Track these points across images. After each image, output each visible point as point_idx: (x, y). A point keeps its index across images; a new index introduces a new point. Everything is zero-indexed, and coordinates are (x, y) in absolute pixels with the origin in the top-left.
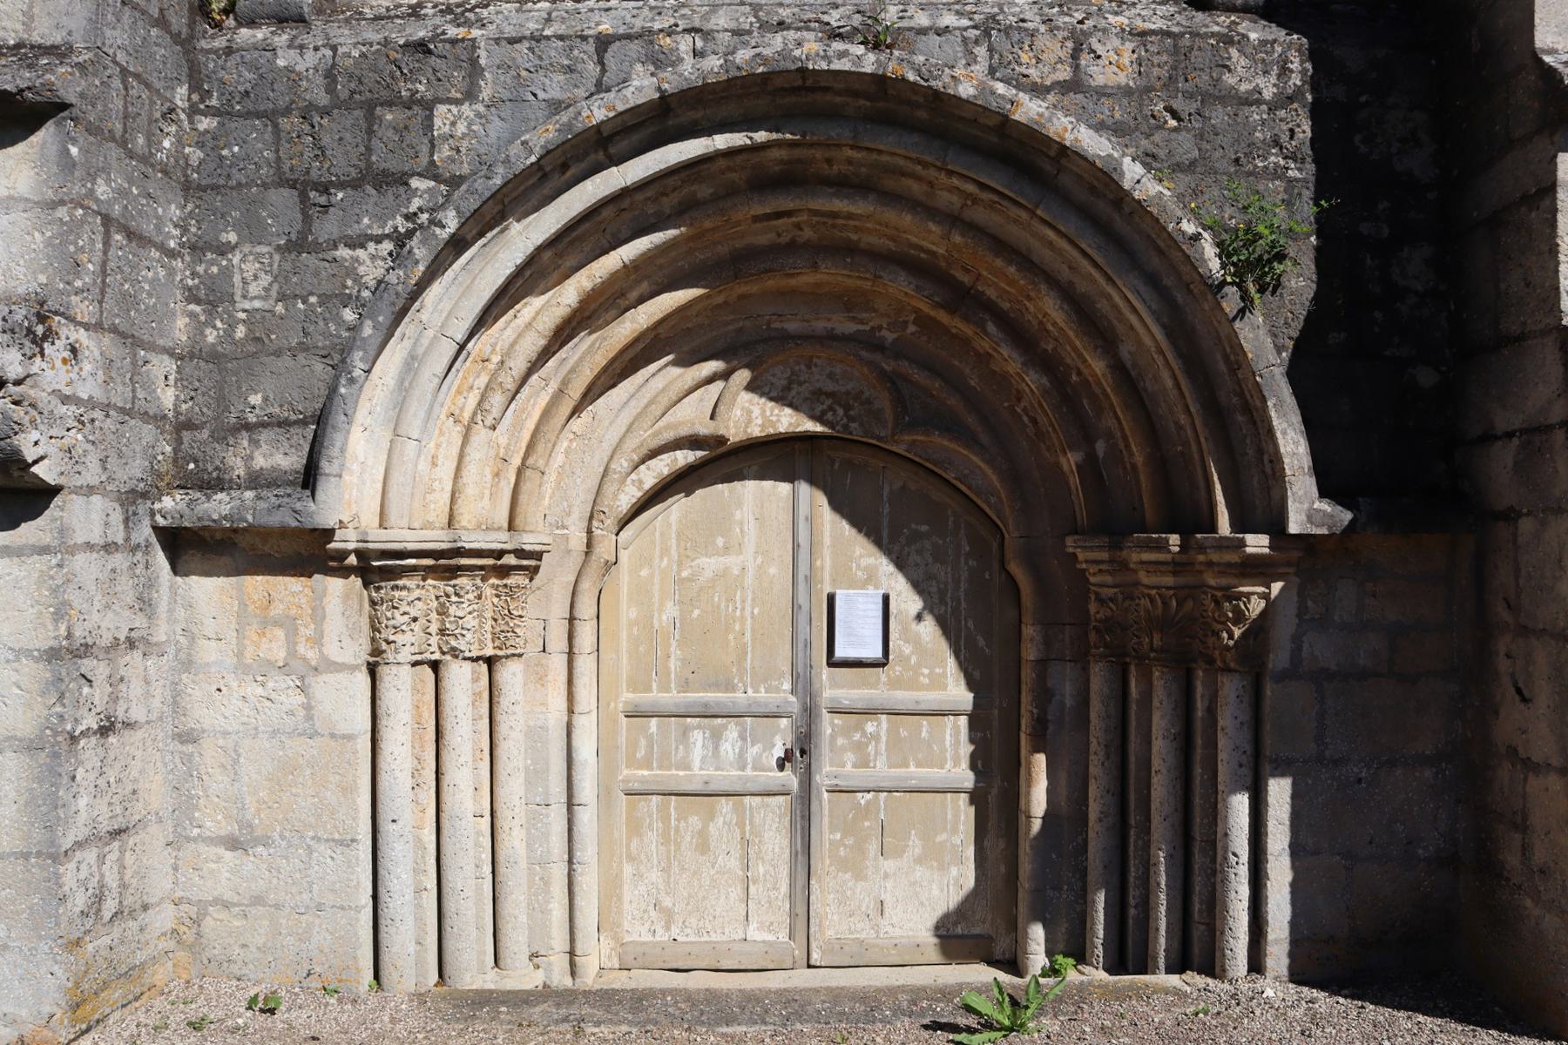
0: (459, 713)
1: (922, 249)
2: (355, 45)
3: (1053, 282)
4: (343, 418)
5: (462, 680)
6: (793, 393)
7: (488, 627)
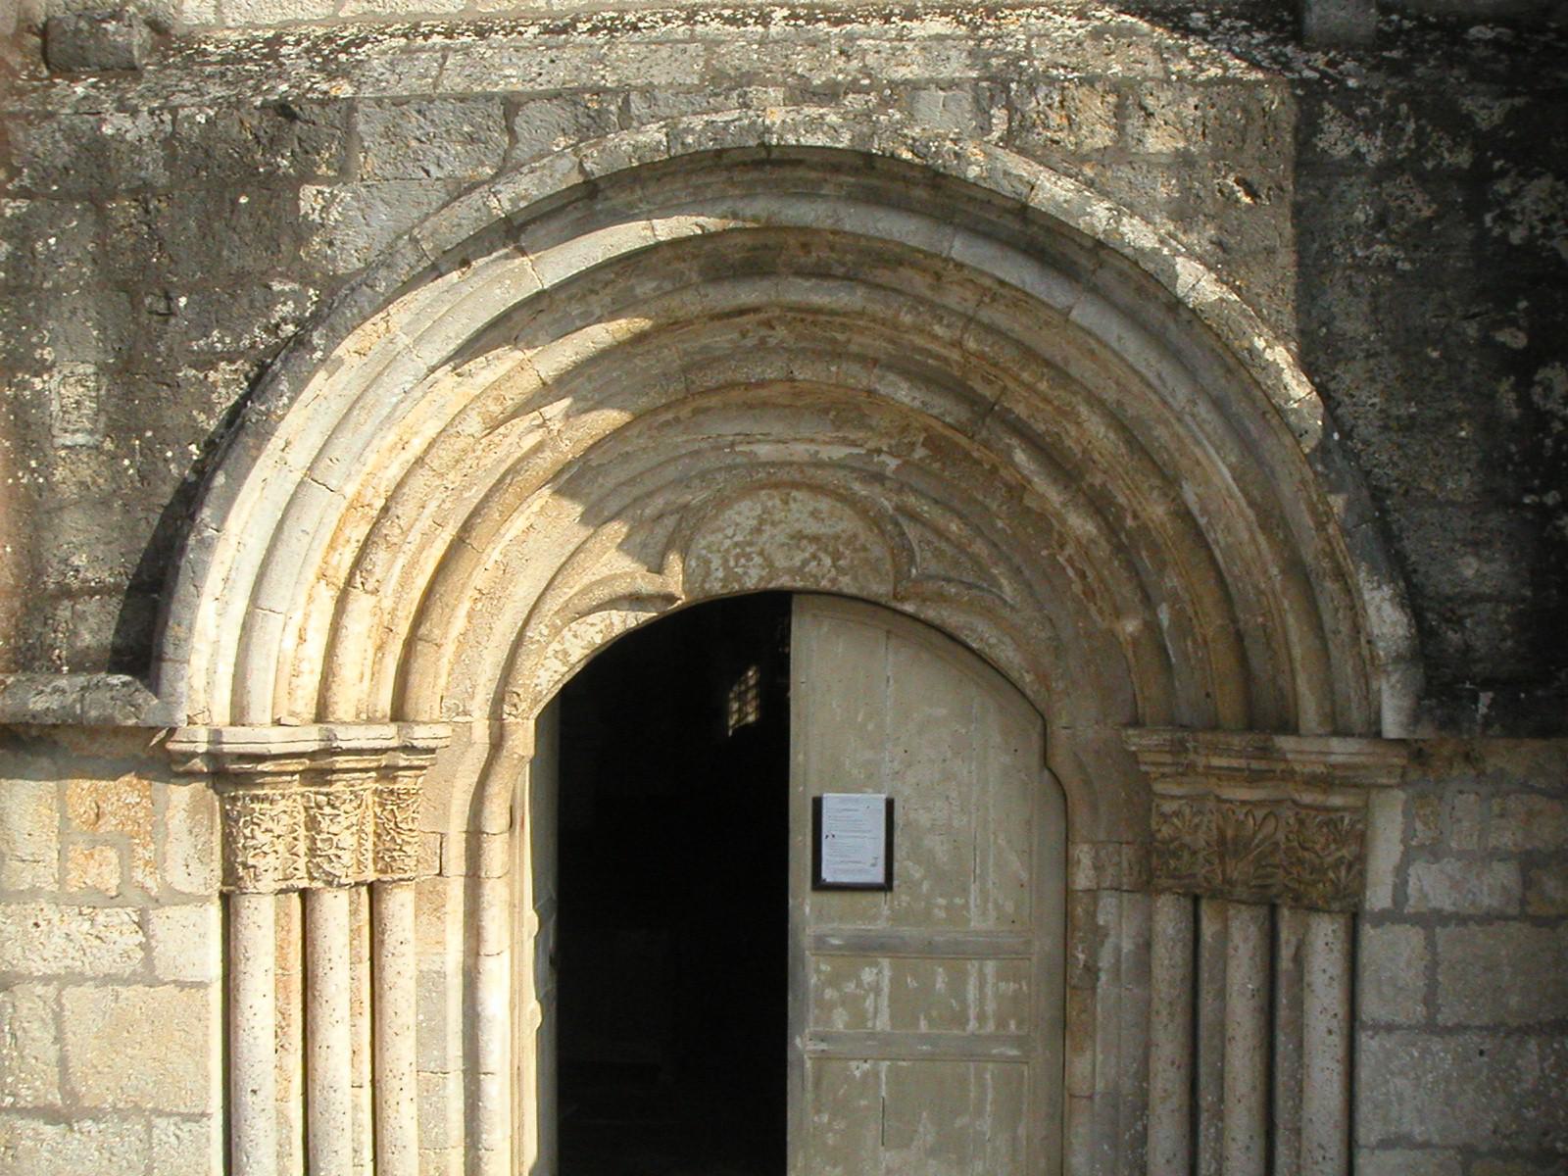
0: (334, 957)
1: (929, 353)
2: (200, 107)
3: (1095, 400)
4: (192, 588)
5: (338, 914)
6: (765, 536)
7: (369, 845)
